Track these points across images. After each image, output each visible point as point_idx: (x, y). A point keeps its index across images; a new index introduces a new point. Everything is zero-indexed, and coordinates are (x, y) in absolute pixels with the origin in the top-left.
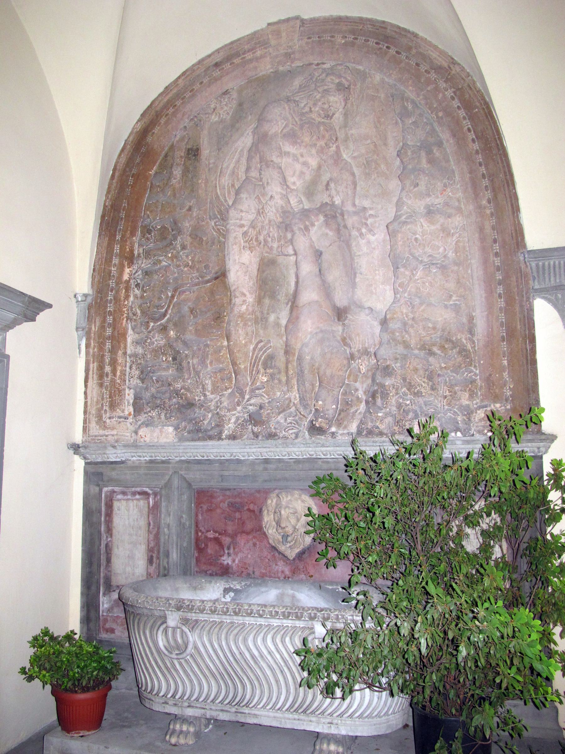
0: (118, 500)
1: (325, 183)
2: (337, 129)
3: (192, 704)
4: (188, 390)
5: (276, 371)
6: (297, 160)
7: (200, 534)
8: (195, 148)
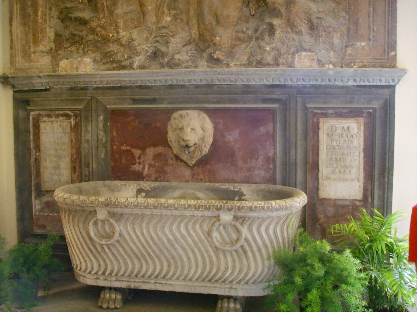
0: (44, 122)
3: (119, 279)
7: (115, 147)
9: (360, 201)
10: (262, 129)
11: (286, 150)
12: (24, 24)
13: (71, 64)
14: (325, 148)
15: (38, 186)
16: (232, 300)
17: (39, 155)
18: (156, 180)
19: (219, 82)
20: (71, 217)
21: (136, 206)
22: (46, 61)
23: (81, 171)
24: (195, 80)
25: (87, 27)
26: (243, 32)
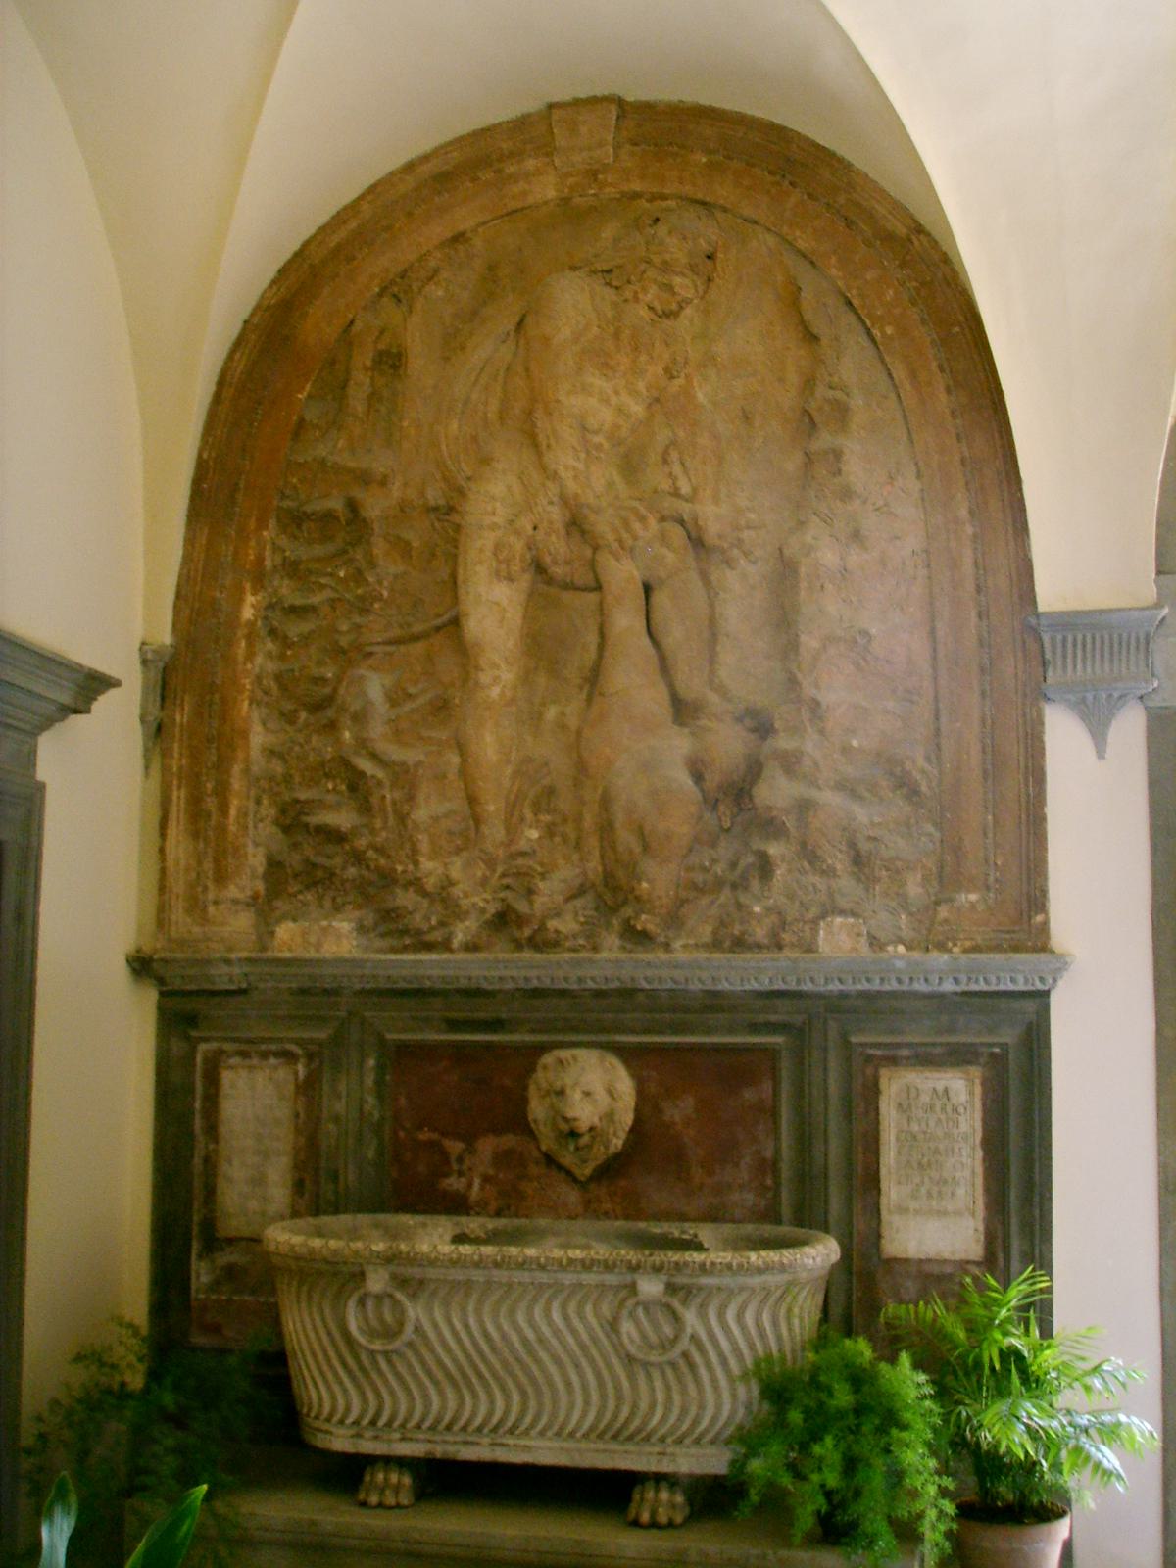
0: (231, 1068)
3: (409, 1435)
8: (394, 350)
10: (749, 1095)
11: (804, 1141)
12: (196, 835)
13: (304, 934)
15: (209, 1225)
16: (664, 1485)
17: (216, 1151)
18: (498, 1214)
19: (649, 983)
20: (305, 1288)
21: (456, 1263)
22: (242, 923)
23: (316, 1190)
24: (593, 979)
25: (343, 848)
26: (705, 870)
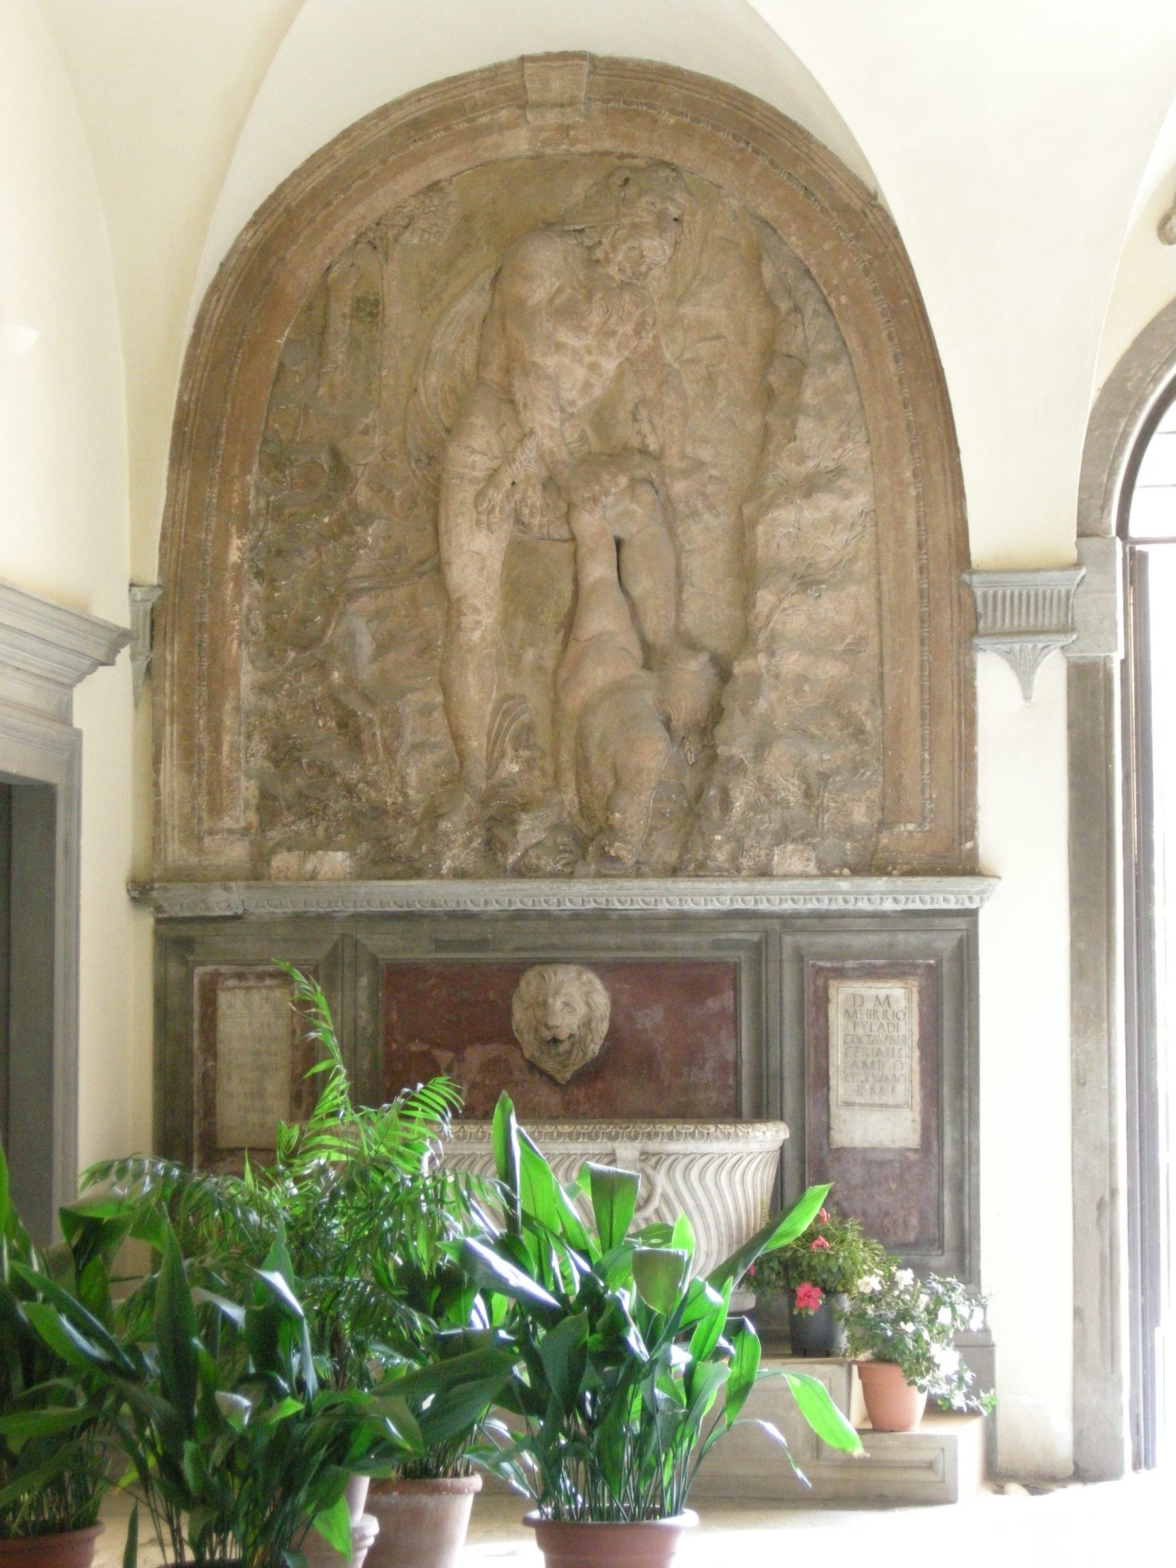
0: (229, 989)
1: (630, 407)
2: (656, 301)
4: (372, 784)
5: (537, 754)
6: (580, 362)
7: (394, 1046)
8: (372, 298)
9: (916, 1151)
10: (712, 1004)
11: (761, 1045)
12: (189, 770)
14: (840, 1041)
17: (214, 1068)
19: (622, 904)
